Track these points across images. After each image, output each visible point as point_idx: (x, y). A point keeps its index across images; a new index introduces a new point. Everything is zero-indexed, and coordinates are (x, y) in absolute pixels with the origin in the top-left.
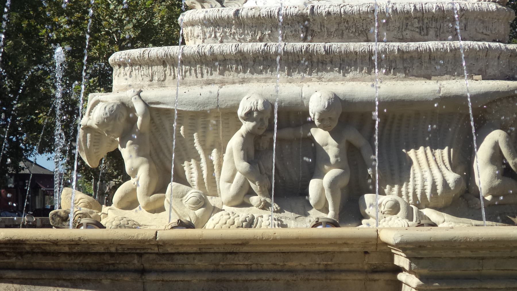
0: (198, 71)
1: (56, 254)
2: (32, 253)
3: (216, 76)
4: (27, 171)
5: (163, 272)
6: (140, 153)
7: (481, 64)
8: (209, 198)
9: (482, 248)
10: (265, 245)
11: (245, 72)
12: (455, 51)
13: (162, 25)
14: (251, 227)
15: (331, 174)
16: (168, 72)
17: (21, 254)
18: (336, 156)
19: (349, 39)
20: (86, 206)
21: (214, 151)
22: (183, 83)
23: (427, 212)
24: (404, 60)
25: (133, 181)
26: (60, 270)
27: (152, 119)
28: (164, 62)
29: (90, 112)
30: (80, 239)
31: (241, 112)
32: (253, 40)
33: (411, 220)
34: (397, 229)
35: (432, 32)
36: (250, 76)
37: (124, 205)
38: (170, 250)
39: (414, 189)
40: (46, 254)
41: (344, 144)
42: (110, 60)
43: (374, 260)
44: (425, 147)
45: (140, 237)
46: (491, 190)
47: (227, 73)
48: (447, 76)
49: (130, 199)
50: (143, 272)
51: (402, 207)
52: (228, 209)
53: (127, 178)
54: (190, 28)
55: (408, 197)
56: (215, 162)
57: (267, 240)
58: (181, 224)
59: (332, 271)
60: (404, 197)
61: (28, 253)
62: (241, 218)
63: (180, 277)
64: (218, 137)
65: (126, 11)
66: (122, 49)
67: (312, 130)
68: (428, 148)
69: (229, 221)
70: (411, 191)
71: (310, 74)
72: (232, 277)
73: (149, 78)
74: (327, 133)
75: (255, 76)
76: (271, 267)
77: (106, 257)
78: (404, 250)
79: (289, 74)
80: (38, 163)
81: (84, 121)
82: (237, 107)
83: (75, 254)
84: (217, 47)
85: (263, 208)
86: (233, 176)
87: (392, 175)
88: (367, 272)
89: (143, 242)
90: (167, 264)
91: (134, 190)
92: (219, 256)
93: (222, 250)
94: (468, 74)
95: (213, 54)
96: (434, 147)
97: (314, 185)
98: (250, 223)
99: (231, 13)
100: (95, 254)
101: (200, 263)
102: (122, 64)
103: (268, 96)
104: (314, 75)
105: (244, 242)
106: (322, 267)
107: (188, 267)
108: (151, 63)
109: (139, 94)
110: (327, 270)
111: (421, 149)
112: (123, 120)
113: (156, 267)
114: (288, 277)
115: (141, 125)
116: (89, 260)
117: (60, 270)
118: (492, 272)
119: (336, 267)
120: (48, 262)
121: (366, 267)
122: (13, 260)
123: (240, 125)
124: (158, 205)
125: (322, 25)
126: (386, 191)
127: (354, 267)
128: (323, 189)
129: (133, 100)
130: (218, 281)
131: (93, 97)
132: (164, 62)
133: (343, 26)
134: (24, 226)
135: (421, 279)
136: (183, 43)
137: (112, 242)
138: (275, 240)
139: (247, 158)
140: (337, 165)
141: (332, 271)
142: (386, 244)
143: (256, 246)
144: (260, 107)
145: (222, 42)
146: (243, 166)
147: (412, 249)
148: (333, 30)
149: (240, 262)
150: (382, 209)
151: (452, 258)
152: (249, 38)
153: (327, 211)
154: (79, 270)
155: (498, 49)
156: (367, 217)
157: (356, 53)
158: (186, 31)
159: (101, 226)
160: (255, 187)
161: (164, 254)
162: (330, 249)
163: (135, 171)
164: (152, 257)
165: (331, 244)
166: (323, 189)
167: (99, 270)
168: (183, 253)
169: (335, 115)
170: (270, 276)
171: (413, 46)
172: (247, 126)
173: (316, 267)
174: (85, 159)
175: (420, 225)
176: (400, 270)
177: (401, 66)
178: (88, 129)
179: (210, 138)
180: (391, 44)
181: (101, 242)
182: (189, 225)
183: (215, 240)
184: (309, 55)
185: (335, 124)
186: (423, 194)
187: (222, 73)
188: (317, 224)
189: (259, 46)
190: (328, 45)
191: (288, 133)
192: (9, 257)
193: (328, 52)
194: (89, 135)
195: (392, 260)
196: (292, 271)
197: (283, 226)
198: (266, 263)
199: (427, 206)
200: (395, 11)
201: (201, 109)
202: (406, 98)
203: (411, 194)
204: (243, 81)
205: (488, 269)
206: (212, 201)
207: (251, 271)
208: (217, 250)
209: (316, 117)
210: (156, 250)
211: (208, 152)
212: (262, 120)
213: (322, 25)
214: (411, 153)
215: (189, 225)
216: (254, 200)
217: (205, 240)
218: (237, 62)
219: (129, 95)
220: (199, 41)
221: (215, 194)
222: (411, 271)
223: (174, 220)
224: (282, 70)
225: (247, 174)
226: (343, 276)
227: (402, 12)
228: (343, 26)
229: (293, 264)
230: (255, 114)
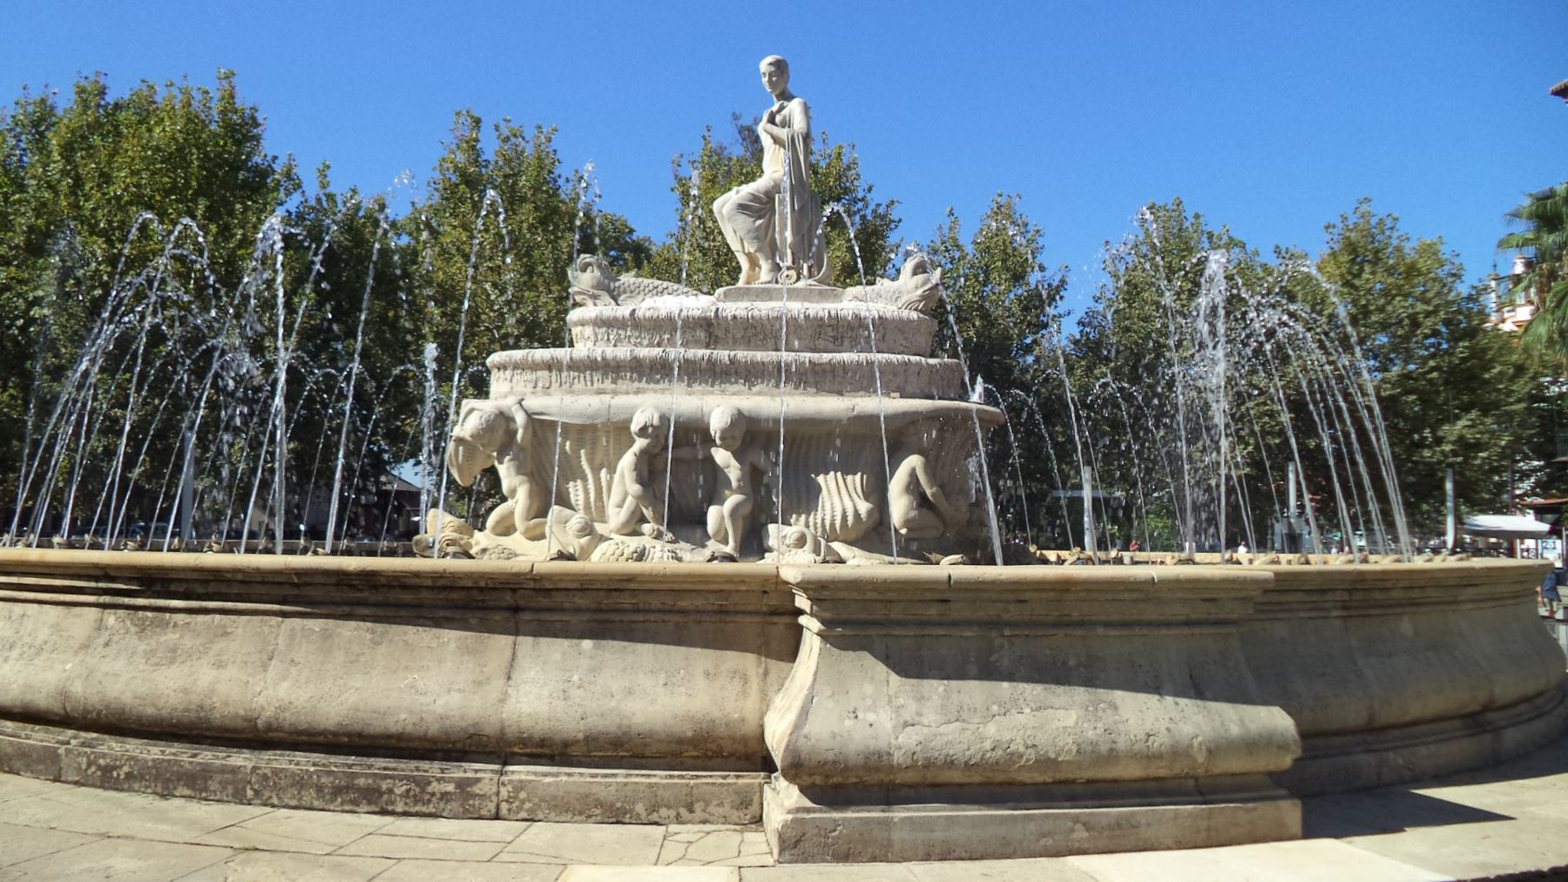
0: (588, 378)
1: (417, 588)
2: (389, 586)
3: (608, 385)
4: (388, 487)
5: (539, 610)
6: (520, 470)
7: (899, 380)
8: (596, 524)
9: (889, 590)
10: (654, 582)
11: (640, 381)
12: (870, 364)
13: (548, 321)
14: (232, 551)
15: (732, 500)
16: (554, 378)
17: (375, 587)
18: (739, 481)
19: (757, 348)
20: (455, 531)
21: (604, 471)
22: (571, 392)
23: (836, 546)
24: (815, 373)
25: (510, 503)
26: (421, 606)
27: (535, 433)
28: (550, 366)
29: (465, 418)
30: (444, 571)
31: (635, 427)
32: (650, 345)
33: (819, 555)
34: (799, 566)
35: (846, 343)
36: (645, 386)
37: (499, 531)
38: (548, 585)
39: (823, 520)
40: (405, 587)
41: (747, 468)
42: (489, 361)
43: (773, 601)
44: (836, 472)
45: (514, 570)
46: (907, 523)
47: (620, 381)
48: (862, 393)
49: (506, 524)
50: (516, 610)
51: (809, 540)
52: (618, 538)
53: (504, 499)
54: (580, 328)
55: (816, 529)
56: (604, 484)
57: (657, 575)
58: (562, 556)
59: (727, 612)
60: (812, 528)
61: (383, 586)
62: (632, 549)
63: (558, 617)
64: (608, 455)
65: (508, 303)
66: (505, 347)
67: (713, 450)
68: (839, 474)
69: (618, 552)
70: (819, 521)
71: (712, 386)
72: (617, 617)
73: (532, 385)
74: (729, 454)
75: (652, 386)
76: (659, 606)
77: (475, 593)
78: (805, 590)
79: (689, 385)
80: (403, 477)
81: (457, 431)
82: (629, 421)
83: (438, 588)
84: (611, 352)
85: (656, 538)
86: (624, 501)
87: (799, 503)
88: (765, 614)
89: (517, 575)
90: (544, 602)
91: (512, 513)
92: (602, 594)
93: (605, 586)
94: (416, 519)
95: (604, 359)
96: (846, 472)
97: (713, 513)
98: (641, 555)
99: (627, 313)
100: (463, 588)
101: (581, 601)
102: (502, 367)
103: (665, 410)
104: (716, 387)
105: (631, 578)
106: (716, 607)
107: (567, 605)
108: (535, 367)
109: (520, 403)
110: (722, 611)
111: (832, 473)
112: (501, 432)
113: (532, 604)
114: (677, 618)
115: (523, 439)
116: (454, 596)
117: (421, 606)
118: (901, 617)
119: (731, 608)
120: (407, 597)
121: (764, 609)
122: (366, 594)
123: (632, 442)
124: (538, 532)
125: (727, 331)
126: (792, 521)
127: (750, 608)
128: (723, 518)
129: (513, 409)
130: (601, 622)
131: (467, 404)
132: (550, 366)
133: (750, 332)
134: (383, 554)
135: (823, 623)
136: (571, 345)
137: (483, 575)
138: (665, 575)
139: (640, 480)
140: (739, 490)
141: (727, 612)
142: (787, 583)
143: (643, 582)
144: (656, 422)
145: (615, 346)
146: (635, 488)
147: (814, 590)
148: (739, 336)
149: (626, 601)
150: (787, 541)
151: (856, 601)
152: (646, 342)
153: (726, 542)
154: (443, 607)
155: (919, 364)
156: (770, 550)
157: (763, 363)
158: (576, 331)
159: (471, 557)
160: (648, 513)
161: (541, 590)
162: (726, 587)
163: (513, 492)
164: (527, 592)
165: (727, 582)
166: (723, 518)
167: (465, 607)
168: (562, 589)
169: (739, 433)
170: (659, 617)
171: (826, 357)
172: (640, 443)
173: (709, 607)
174: (456, 476)
175: (825, 562)
176: (801, 612)
177: (811, 380)
178: (460, 441)
179: (599, 457)
180: (802, 354)
181: (469, 575)
182: (571, 558)
183: (597, 575)
184: (712, 363)
185: (737, 444)
186: (833, 524)
187: (614, 382)
188: (712, 558)
189: (656, 352)
190: (732, 353)
191: (685, 453)
192: (361, 591)
193: (732, 361)
194: (461, 448)
195: (793, 601)
196: (682, 612)
197: (680, 560)
198: (655, 602)
199: (836, 540)
200: (807, 317)
201: (589, 422)
202: (817, 416)
203: (819, 525)
204: (637, 392)
205: (896, 613)
206: (600, 528)
207: (638, 611)
208: (599, 586)
209: (718, 435)
210: (532, 585)
211: (596, 471)
212: (657, 436)
213: (727, 331)
214: (821, 479)
215: (571, 558)
216: (647, 528)
217: (586, 575)
218: (632, 370)
219: (509, 403)
220: (590, 344)
221: (603, 519)
222: (812, 614)
223: (554, 551)
224: (680, 379)
225: (638, 498)
226: (739, 618)
227: (815, 318)
228: (750, 332)
229: (684, 603)
230: (650, 430)
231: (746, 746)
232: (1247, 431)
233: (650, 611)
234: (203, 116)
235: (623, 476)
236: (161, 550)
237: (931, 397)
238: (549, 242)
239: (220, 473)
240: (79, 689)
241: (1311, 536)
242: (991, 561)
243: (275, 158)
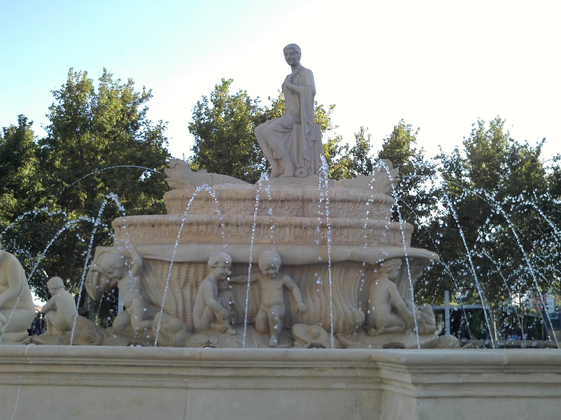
29: (98, 257)
234: (412, 134)
235: (430, 315)
238: (257, 149)
240: (283, 196)
242: (255, 347)
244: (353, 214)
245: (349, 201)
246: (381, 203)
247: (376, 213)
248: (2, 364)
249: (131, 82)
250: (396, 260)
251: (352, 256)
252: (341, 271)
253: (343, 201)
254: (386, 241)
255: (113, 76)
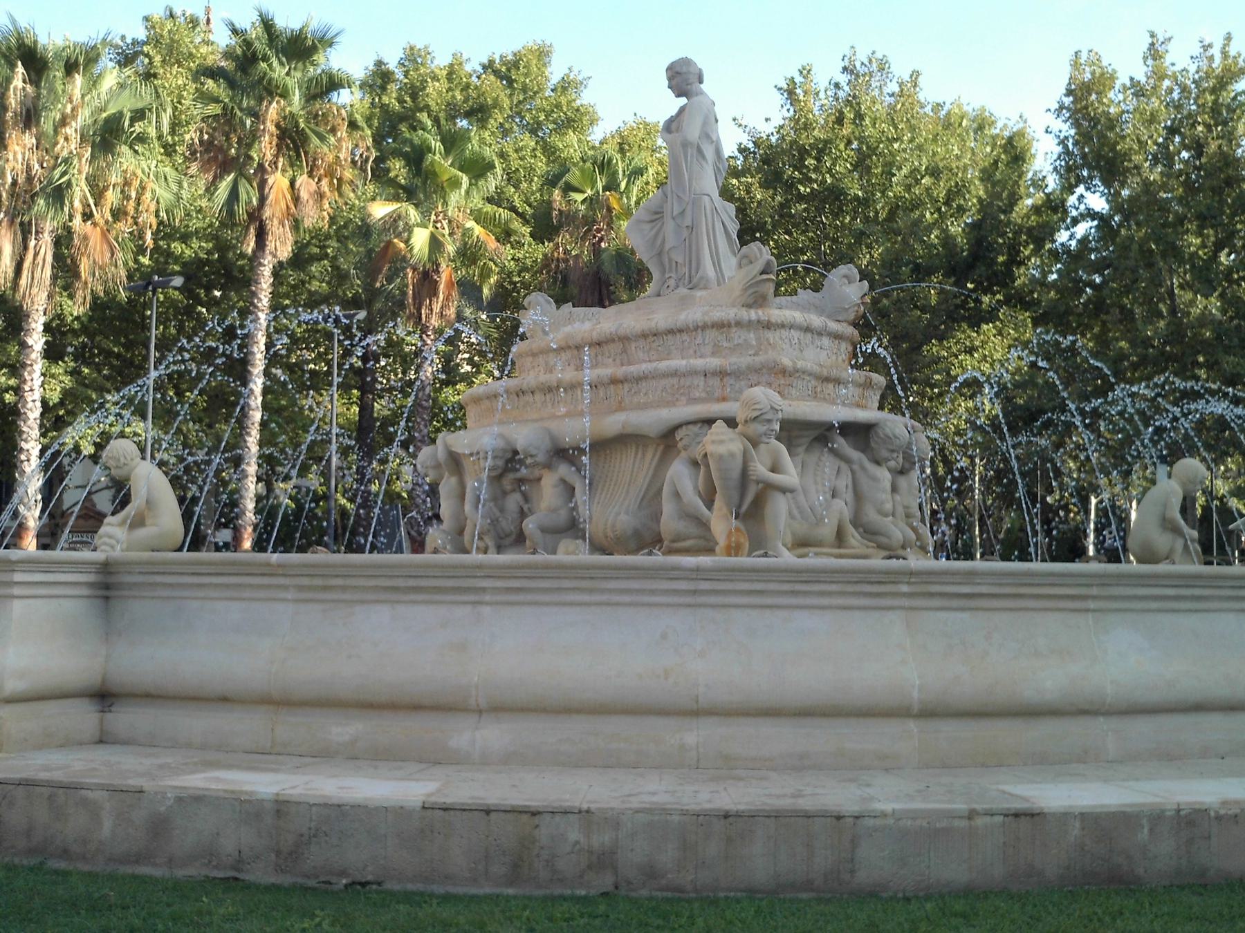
91: (789, 475)
231: (697, 702)
232: (115, 919)
233: (1097, 585)
236: (363, 552)
237: (135, 877)
239: (95, 390)
241: (492, 549)
243: (468, 60)
244: (691, 351)
245: (681, 331)
246: (729, 326)
247: (725, 344)
248: (1231, 707)
249: (1154, 53)
250: (690, 427)
251: (623, 427)
252: (636, 454)
253: (671, 332)
254: (703, 395)
255: (921, 80)
